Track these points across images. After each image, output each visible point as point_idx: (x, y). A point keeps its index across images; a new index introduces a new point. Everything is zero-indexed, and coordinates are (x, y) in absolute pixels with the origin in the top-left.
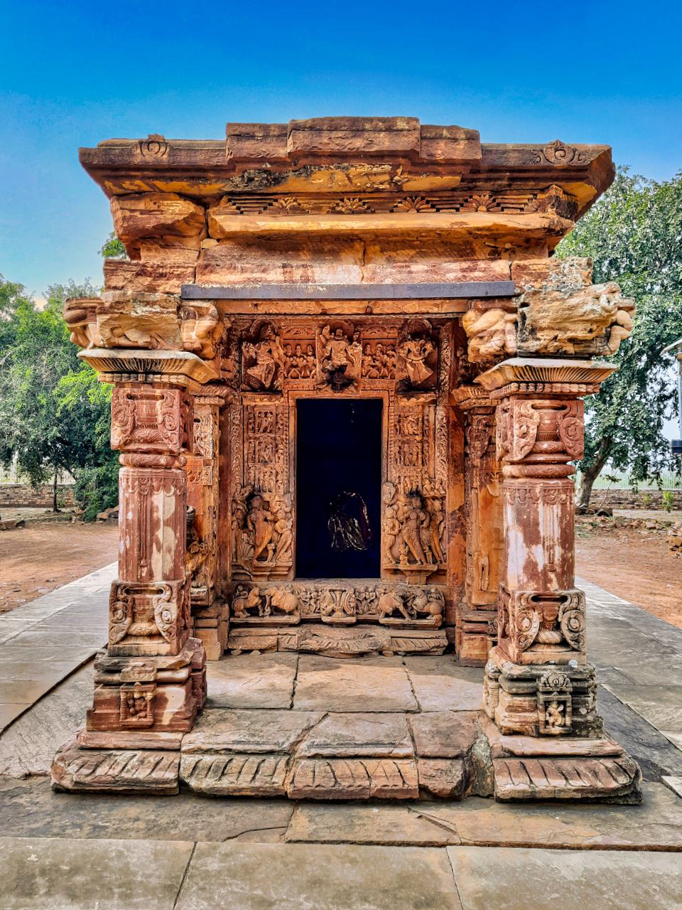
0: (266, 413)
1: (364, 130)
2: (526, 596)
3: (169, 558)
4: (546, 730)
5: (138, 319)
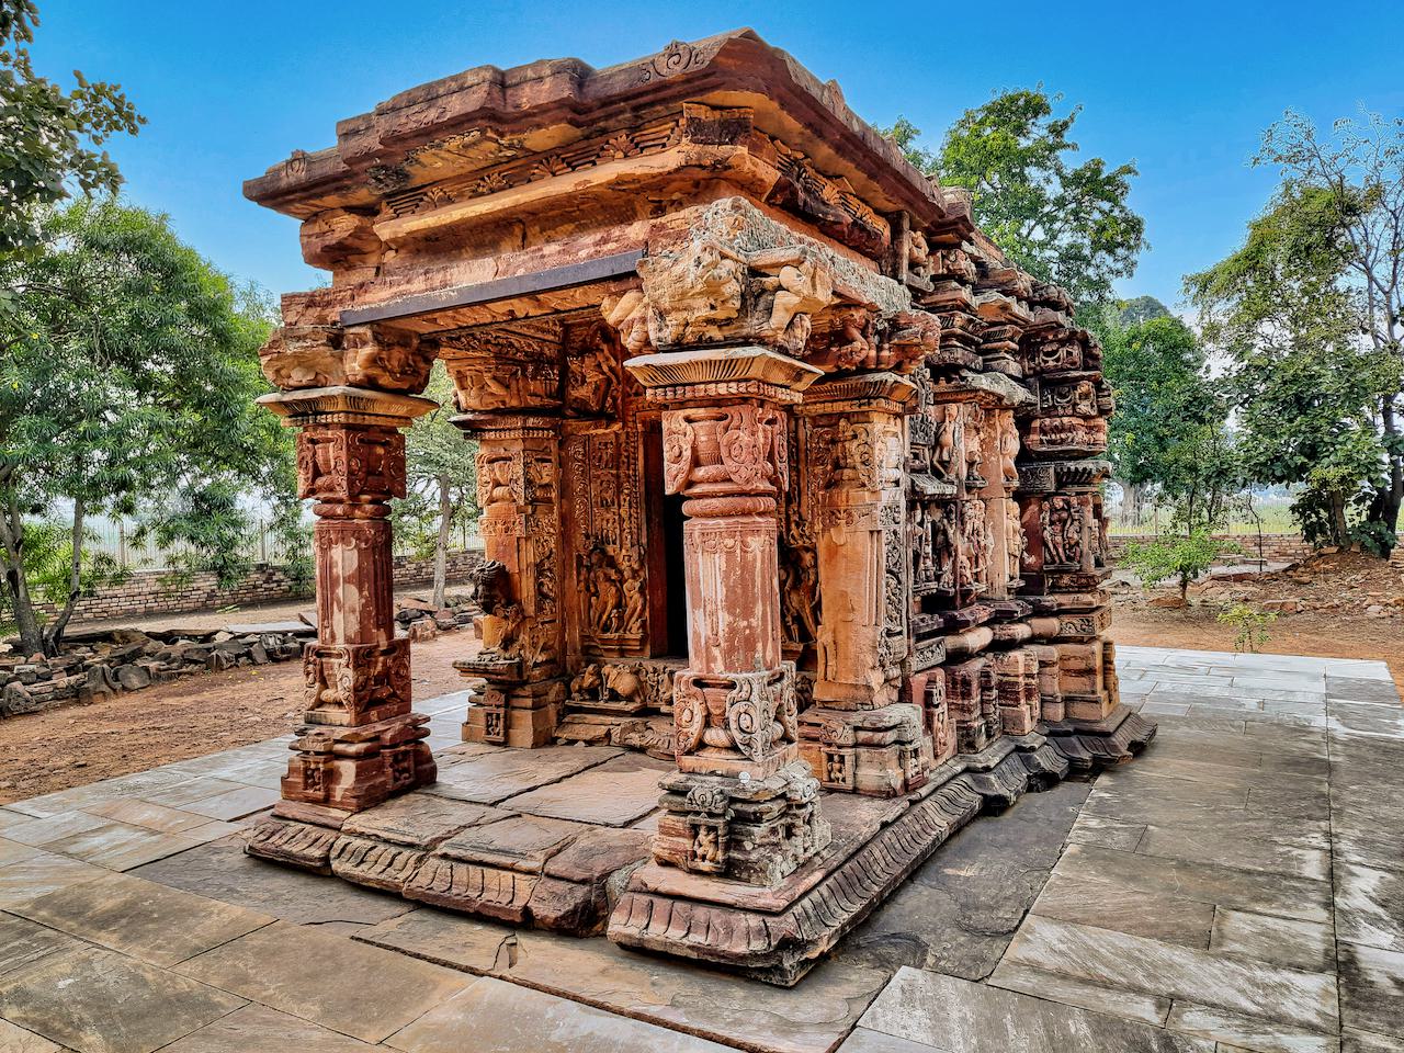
0: (606, 444)
1: (438, 97)
2: (685, 679)
3: (354, 620)
4: (694, 864)
5: (295, 356)
